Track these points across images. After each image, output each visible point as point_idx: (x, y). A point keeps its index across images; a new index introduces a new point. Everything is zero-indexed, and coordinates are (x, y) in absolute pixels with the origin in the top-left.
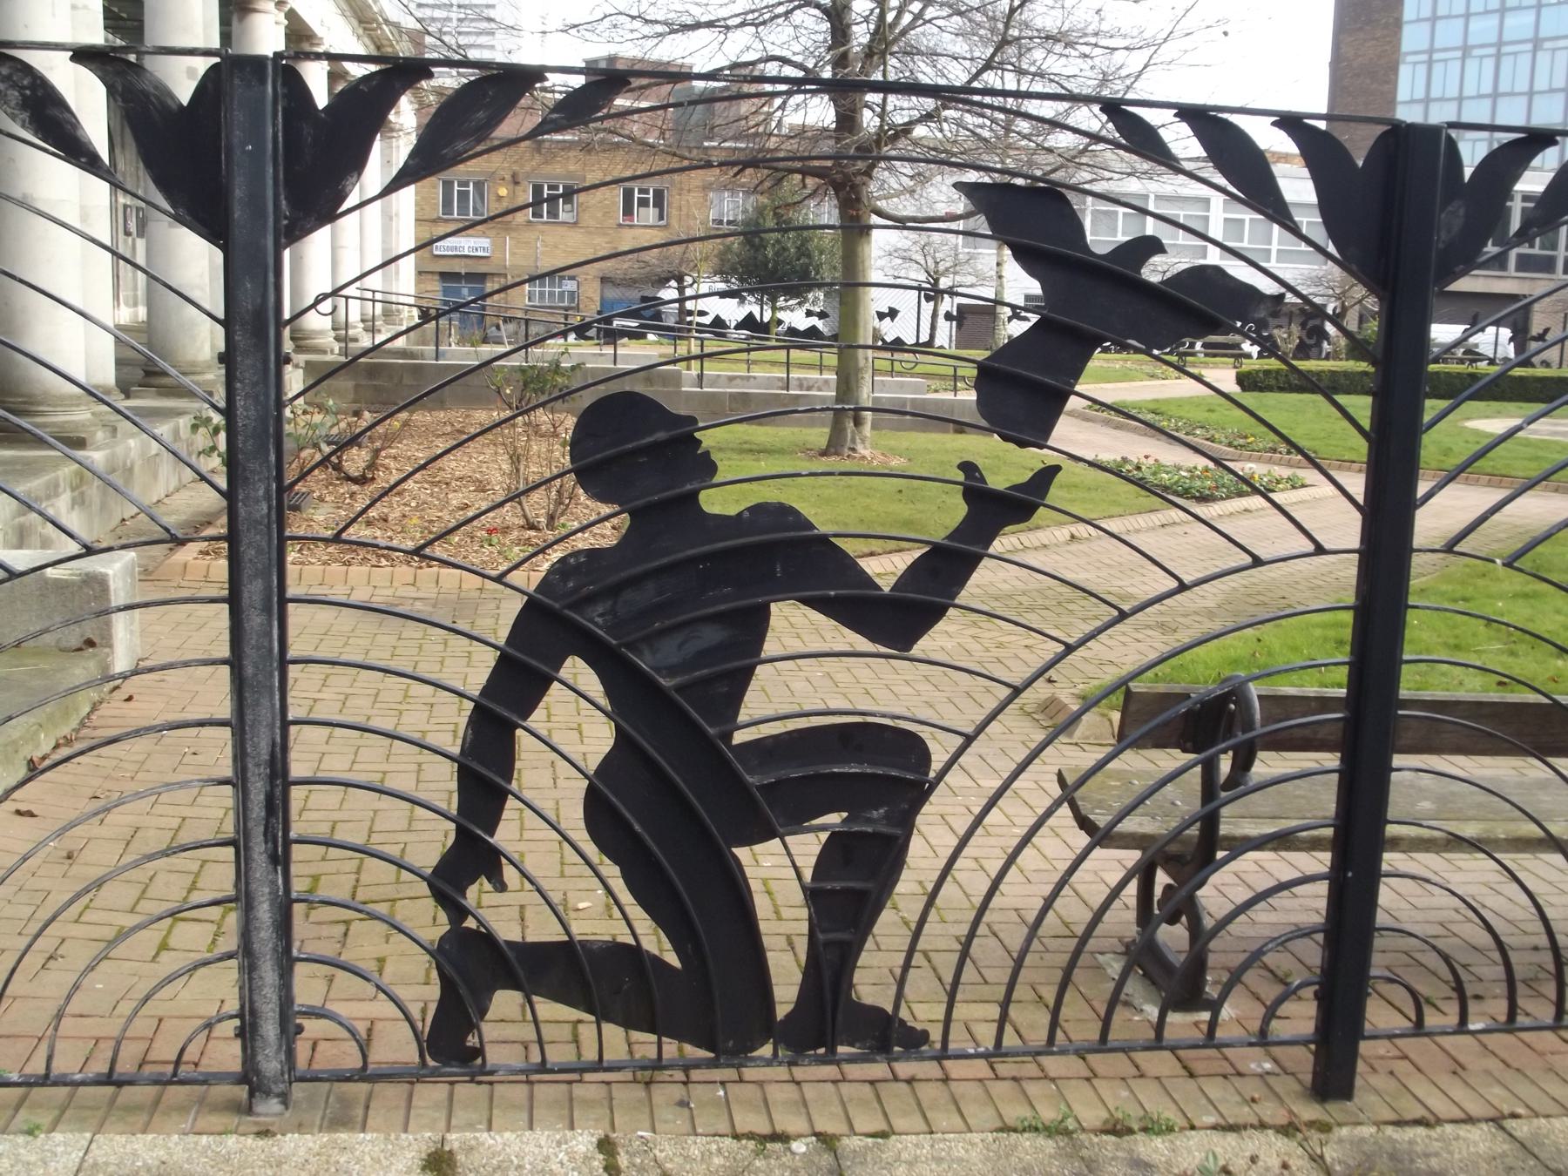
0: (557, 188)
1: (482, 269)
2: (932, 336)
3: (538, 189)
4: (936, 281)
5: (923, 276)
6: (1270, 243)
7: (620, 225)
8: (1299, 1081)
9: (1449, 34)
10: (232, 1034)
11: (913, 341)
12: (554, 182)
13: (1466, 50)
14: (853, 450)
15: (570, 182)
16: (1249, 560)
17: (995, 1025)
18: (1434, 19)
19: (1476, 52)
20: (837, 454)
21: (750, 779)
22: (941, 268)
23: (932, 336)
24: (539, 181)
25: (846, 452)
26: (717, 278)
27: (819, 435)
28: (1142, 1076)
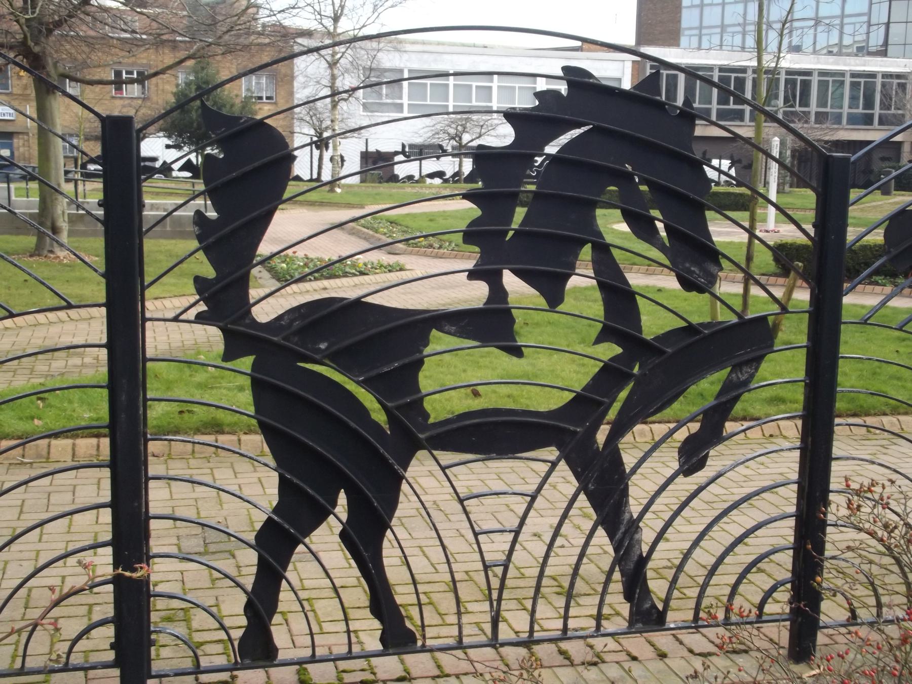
0: (132, 73)
1: (10, 129)
2: (319, 174)
3: (118, 74)
4: (321, 134)
5: (312, 132)
6: (447, 100)
7: (113, 97)
8: (106, 666)
9: (712, 16)
10: (109, 647)
11: (308, 178)
12: (130, 69)
13: (723, 27)
14: (51, 252)
15: (141, 69)
16: (7, 314)
17: (28, 653)
18: (702, 6)
19: (730, 29)
20: (39, 255)
21: (421, 436)
22: (324, 126)
23: (319, 174)
24: (118, 68)
25: (45, 252)
26: (161, 134)
27: (30, 241)
28: (437, 572)
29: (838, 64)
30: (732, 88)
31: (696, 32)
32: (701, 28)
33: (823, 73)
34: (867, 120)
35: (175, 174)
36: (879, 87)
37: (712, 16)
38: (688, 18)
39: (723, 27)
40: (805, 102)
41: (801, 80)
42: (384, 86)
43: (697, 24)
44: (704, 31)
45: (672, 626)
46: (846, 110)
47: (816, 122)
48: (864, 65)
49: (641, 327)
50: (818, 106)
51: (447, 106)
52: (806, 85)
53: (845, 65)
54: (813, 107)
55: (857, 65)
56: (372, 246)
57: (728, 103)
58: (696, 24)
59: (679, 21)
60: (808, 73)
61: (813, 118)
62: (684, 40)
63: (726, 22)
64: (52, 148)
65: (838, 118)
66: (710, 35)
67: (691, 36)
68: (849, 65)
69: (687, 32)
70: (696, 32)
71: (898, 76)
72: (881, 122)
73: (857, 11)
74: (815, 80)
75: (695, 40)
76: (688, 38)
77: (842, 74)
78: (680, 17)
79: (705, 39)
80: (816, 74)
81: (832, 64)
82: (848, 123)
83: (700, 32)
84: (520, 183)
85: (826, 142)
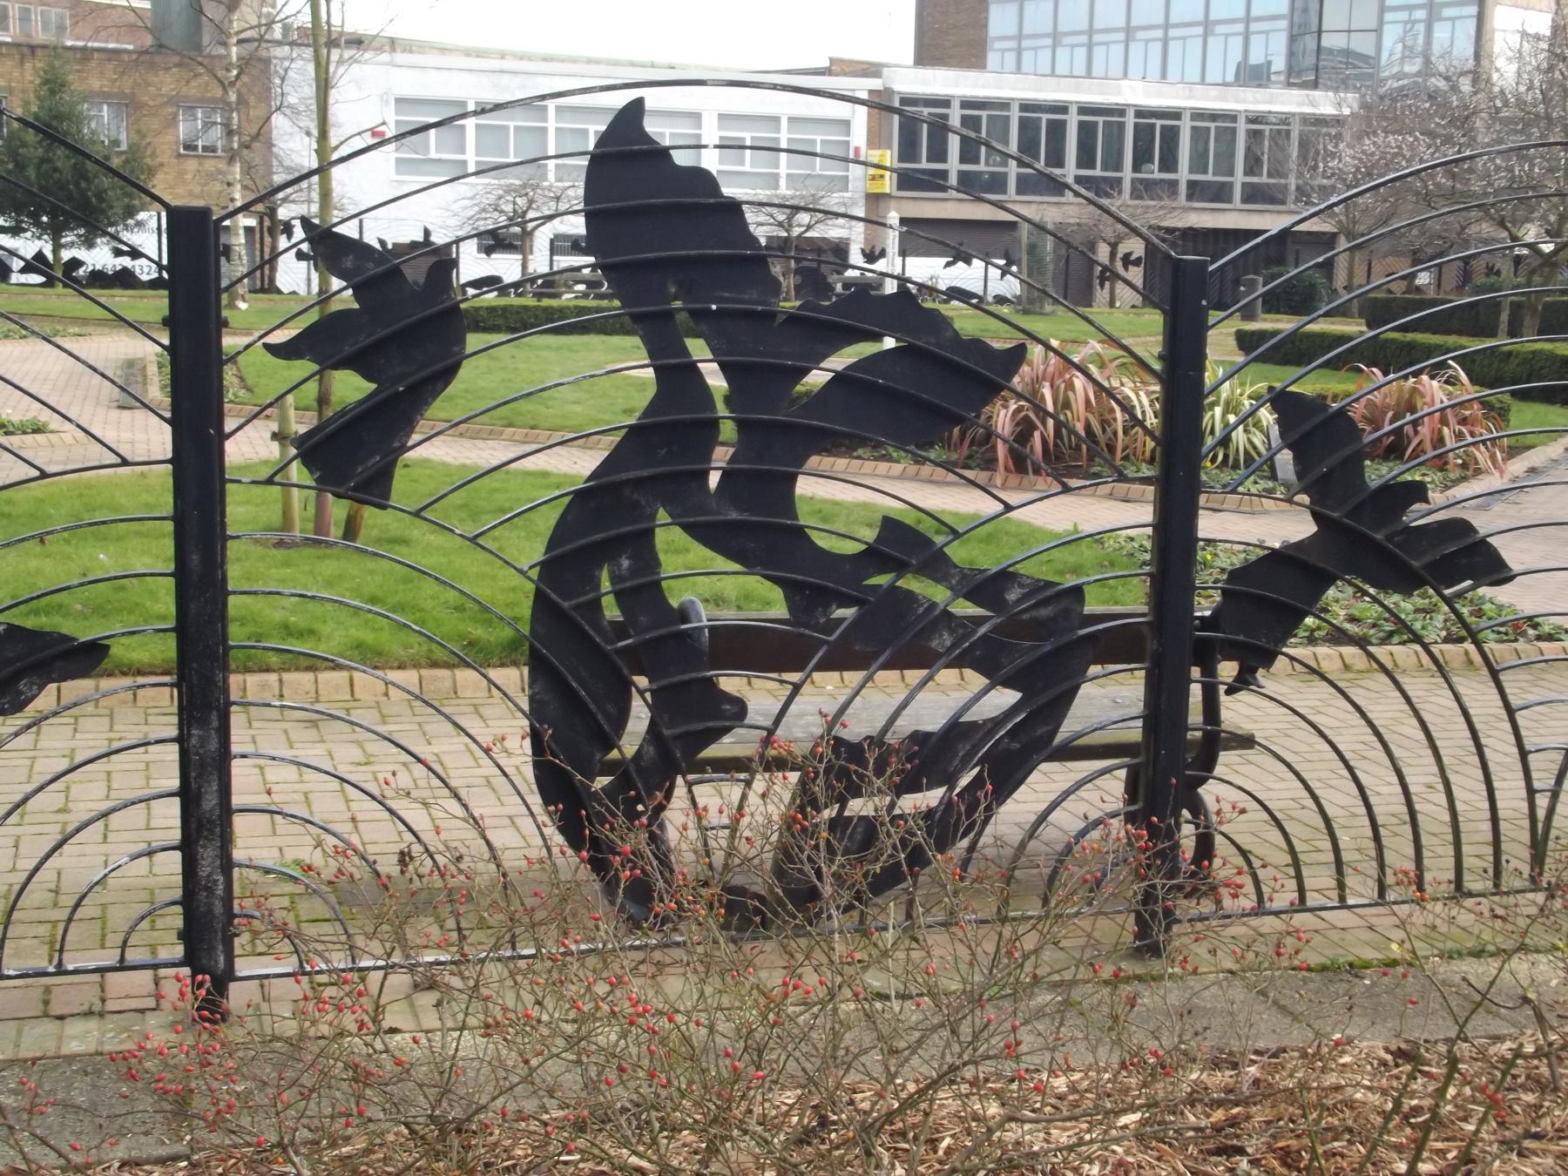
9: (1038, 17)
13: (1129, 31)
29: (1225, 100)
30: (984, 135)
31: (1012, 44)
32: (1020, 37)
33: (1198, 115)
34: (1219, 194)
35: (15, 278)
36: (1295, 135)
37: (1038, 17)
38: (1000, 21)
39: (1056, 37)
40: (1169, 163)
41: (1163, 127)
42: (433, 131)
43: (1013, 31)
44: (1254, 27)
45: (12, 973)
46: (1239, 178)
47: (1019, 192)
48: (1270, 102)
49: (389, 492)
50: (1191, 171)
51: (464, 163)
52: (1171, 136)
53: (1237, 101)
54: (1184, 174)
55: (1257, 102)
56: (242, 420)
57: (976, 161)
58: (1012, 30)
59: (985, 26)
60: (1063, 108)
61: (1183, 188)
62: (992, 58)
63: (1213, 16)
64: (107, 330)
65: (998, 183)
66: (1035, 49)
67: (1004, 50)
68: (1244, 101)
69: (997, 45)
70: (1084, 39)
71: (1214, 116)
72: (1247, 199)
73: (1272, 11)
74: (1186, 127)
75: (1010, 58)
76: (1068, 50)
77: (1232, 117)
78: (987, 18)
79: (1027, 57)
80: (1187, 117)
81: (1215, 99)
82: (1019, 192)
83: (1247, 27)
84: (1360, 438)
85: (1170, 230)
